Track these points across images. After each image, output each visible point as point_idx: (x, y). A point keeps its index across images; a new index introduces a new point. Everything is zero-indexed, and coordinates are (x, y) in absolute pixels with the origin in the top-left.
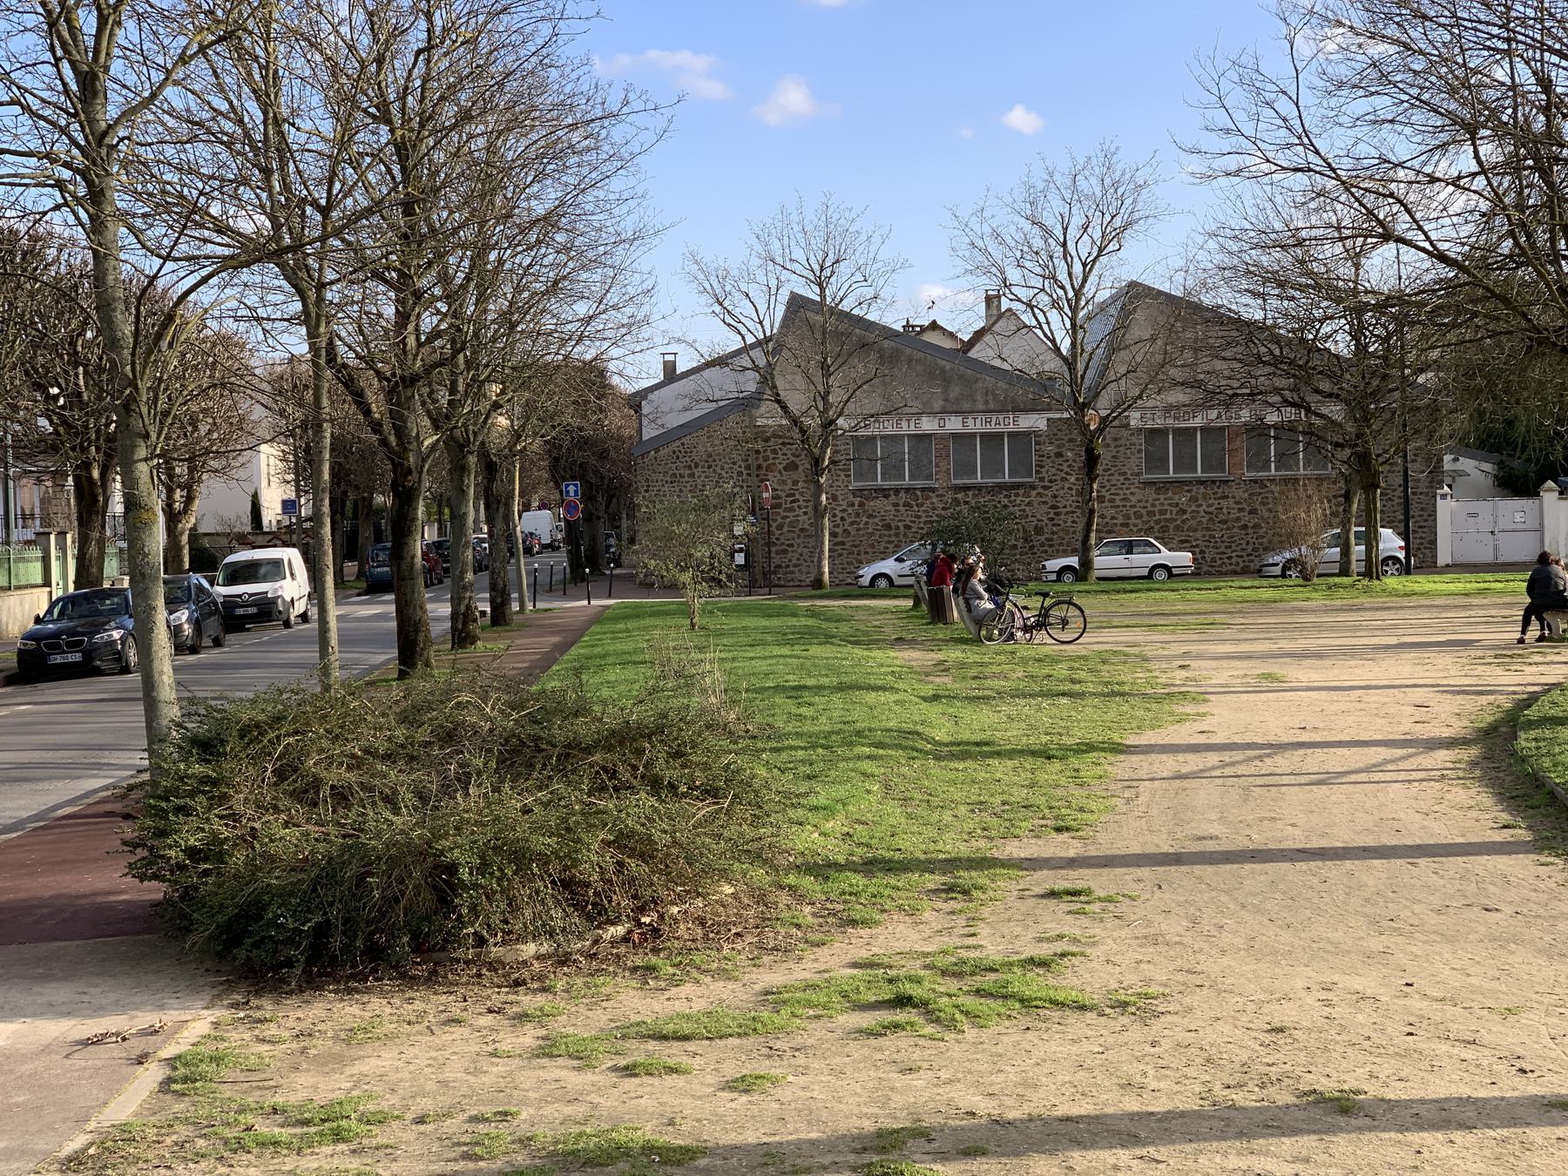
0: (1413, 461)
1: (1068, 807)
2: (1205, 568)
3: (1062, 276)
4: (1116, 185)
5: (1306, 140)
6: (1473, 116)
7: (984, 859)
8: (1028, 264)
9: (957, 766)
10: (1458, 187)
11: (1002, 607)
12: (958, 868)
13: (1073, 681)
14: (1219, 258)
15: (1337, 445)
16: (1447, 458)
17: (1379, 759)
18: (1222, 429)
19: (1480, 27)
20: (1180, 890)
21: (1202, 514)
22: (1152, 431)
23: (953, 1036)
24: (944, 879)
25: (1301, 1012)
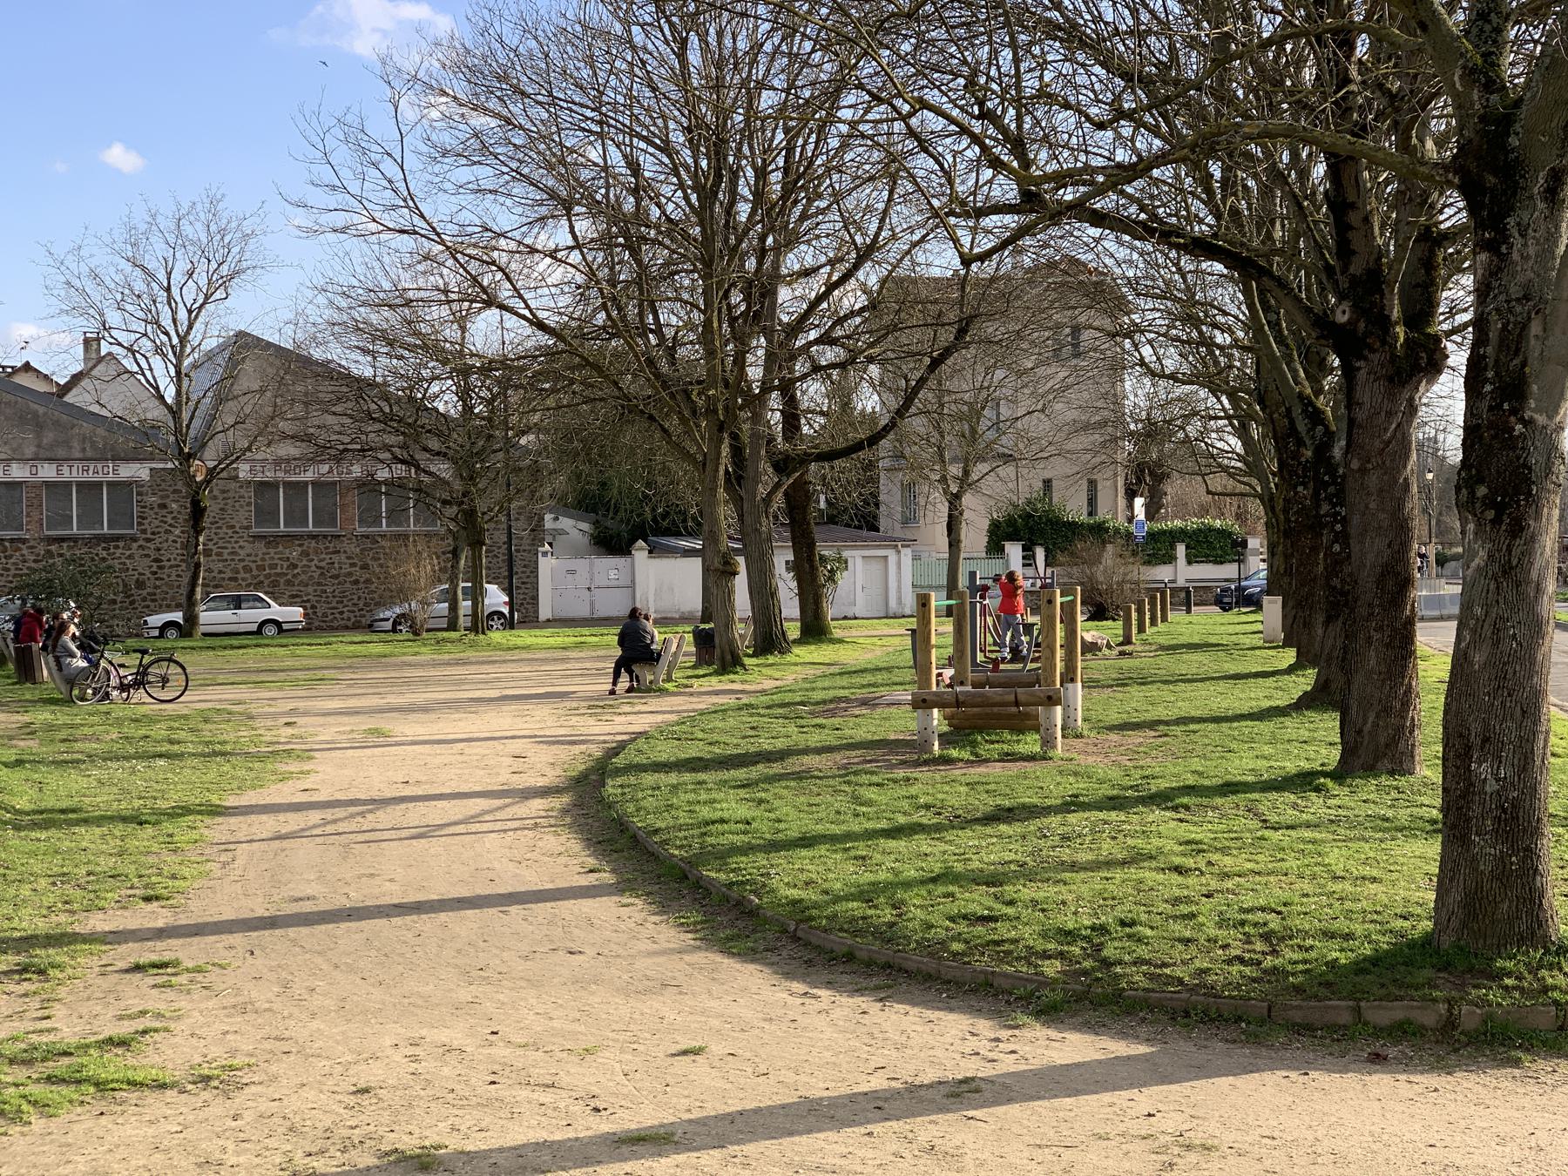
0: (517, 519)
1: (159, 875)
2: (317, 624)
3: (166, 322)
4: (223, 232)
5: (411, 203)
6: (569, 195)
7: (63, 935)
8: (129, 307)
9: (39, 835)
10: (555, 258)
11: (97, 665)
12: (33, 946)
13: (172, 742)
14: (329, 313)
15: (445, 502)
16: (548, 517)
17: (478, 810)
18: (334, 483)
19: (574, 108)
20: (273, 955)
21: (314, 568)
22: (262, 483)
23: (18, 1129)
24: (17, 959)
25: (384, 1072)
